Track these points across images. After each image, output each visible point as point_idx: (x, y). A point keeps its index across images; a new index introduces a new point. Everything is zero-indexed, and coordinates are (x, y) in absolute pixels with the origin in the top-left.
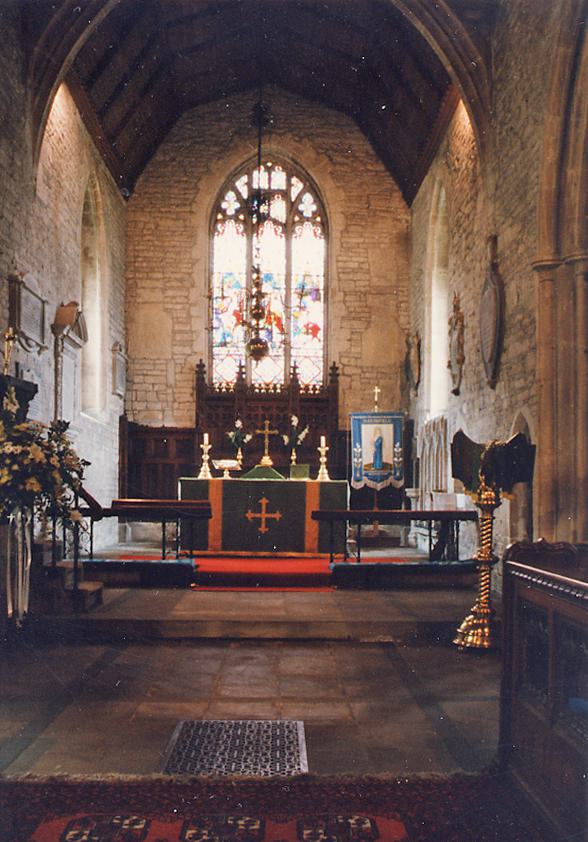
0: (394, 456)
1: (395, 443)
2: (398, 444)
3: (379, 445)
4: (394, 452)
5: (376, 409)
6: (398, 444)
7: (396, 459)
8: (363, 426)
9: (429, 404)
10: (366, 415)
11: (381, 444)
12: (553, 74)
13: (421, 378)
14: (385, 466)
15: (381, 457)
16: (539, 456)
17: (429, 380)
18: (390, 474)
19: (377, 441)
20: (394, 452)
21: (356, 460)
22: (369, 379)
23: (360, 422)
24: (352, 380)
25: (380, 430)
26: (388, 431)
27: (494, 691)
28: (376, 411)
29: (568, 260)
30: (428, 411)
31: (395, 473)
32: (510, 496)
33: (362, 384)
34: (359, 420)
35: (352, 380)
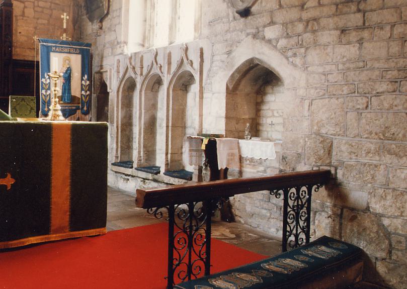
0: (82, 90)
1: (83, 75)
2: (86, 76)
3: (68, 78)
4: (82, 85)
5: (64, 37)
6: (86, 76)
7: (83, 92)
8: (52, 55)
9: (126, 35)
10: (56, 42)
11: (70, 76)
12: (367, 160)
13: (110, 10)
14: (73, 99)
15: (69, 89)
16: (280, 158)
17: (127, 11)
18: (78, 108)
19: (67, 71)
20: (82, 85)
21: (44, 92)
22: (43, 8)
23: (48, 50)
24: (25, 7)
25: (69, 60)
26: (76, 61)
27: (238, 197)
28: (65, 39)
29: (150, 176)
30: (126, 43)
31: (83, 108)
32: (354, 3)
33: (35, 11)
34: (48, 47)
35: (25, 7)
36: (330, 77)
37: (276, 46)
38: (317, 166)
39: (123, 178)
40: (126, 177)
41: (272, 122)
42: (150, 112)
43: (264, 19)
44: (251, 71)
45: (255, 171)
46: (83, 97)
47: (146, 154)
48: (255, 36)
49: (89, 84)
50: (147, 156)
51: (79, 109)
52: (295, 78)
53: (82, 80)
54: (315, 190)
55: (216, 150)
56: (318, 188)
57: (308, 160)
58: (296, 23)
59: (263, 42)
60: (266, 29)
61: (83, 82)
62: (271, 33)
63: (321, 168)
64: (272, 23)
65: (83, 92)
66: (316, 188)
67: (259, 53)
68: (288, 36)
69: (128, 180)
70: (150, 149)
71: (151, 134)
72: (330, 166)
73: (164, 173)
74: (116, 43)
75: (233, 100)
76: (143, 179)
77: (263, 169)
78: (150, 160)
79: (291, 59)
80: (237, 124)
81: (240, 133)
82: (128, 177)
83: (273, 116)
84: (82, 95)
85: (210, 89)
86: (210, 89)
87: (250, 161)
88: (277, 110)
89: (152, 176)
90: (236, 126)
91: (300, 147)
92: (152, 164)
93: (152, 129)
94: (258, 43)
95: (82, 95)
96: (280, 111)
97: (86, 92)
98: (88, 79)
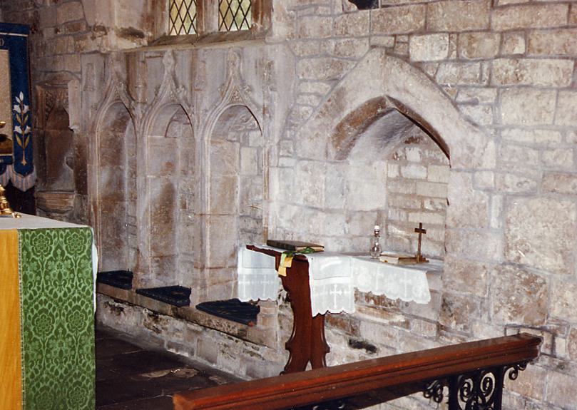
0: (15, 123)
1: (14, 93)
7: (18, 129)
20: (14, 112)
36: (549, 156)
37: (435, 77)
38: (514, 327)
39: (110, 306)
40: (117, 304)
41: (421, 224)
42: (163, 178)
43: (409, 18)
44: (378, 121)
45: (386, 322)
46: (18, 139)
47: (157, 261)
48: (390, 52)
49: (28, 112)
50: (159, 266)
51: (11, 164)
52: (471, 149)
53: (14, 102)
54: (510, 375)
55: (309, 279)
56: (516, 372)
57: (496, 312)
58: (479, 35)
59: (407, 66)
60: (413, 39)
61: (17, 108)
62: (421, 49)
63: (522, 331)
64: (426, 30)
65: (18, 129)
66: (513, 372)
67: (398, 89)
68: (460, 61)
69: (122, 309)
70: (165, 252)
71: (167, 222)
72: (542, 329)
73: (196, 306)
74: (84, 28)
75: (340, 175)
76: (154, 312)
77: (403, 320)
78: (166, 275)
79: (466, 111)
80: (347, 222)
81: (355, 239)
82: (121, 305)
83: (423, 210)
84: (15, 134)
85: (292, 150)
86: (292, 150)
87: (375, 302)
88: (430, 198)
89: (173, 309)
90: (346, 226)
91: (481, 286)
92: (171, 253)
93: (167, 212)
94: (394, 67)
95: (15, 134)
96: (437, 202)
97: (23, 128)
98: (27, 101)
